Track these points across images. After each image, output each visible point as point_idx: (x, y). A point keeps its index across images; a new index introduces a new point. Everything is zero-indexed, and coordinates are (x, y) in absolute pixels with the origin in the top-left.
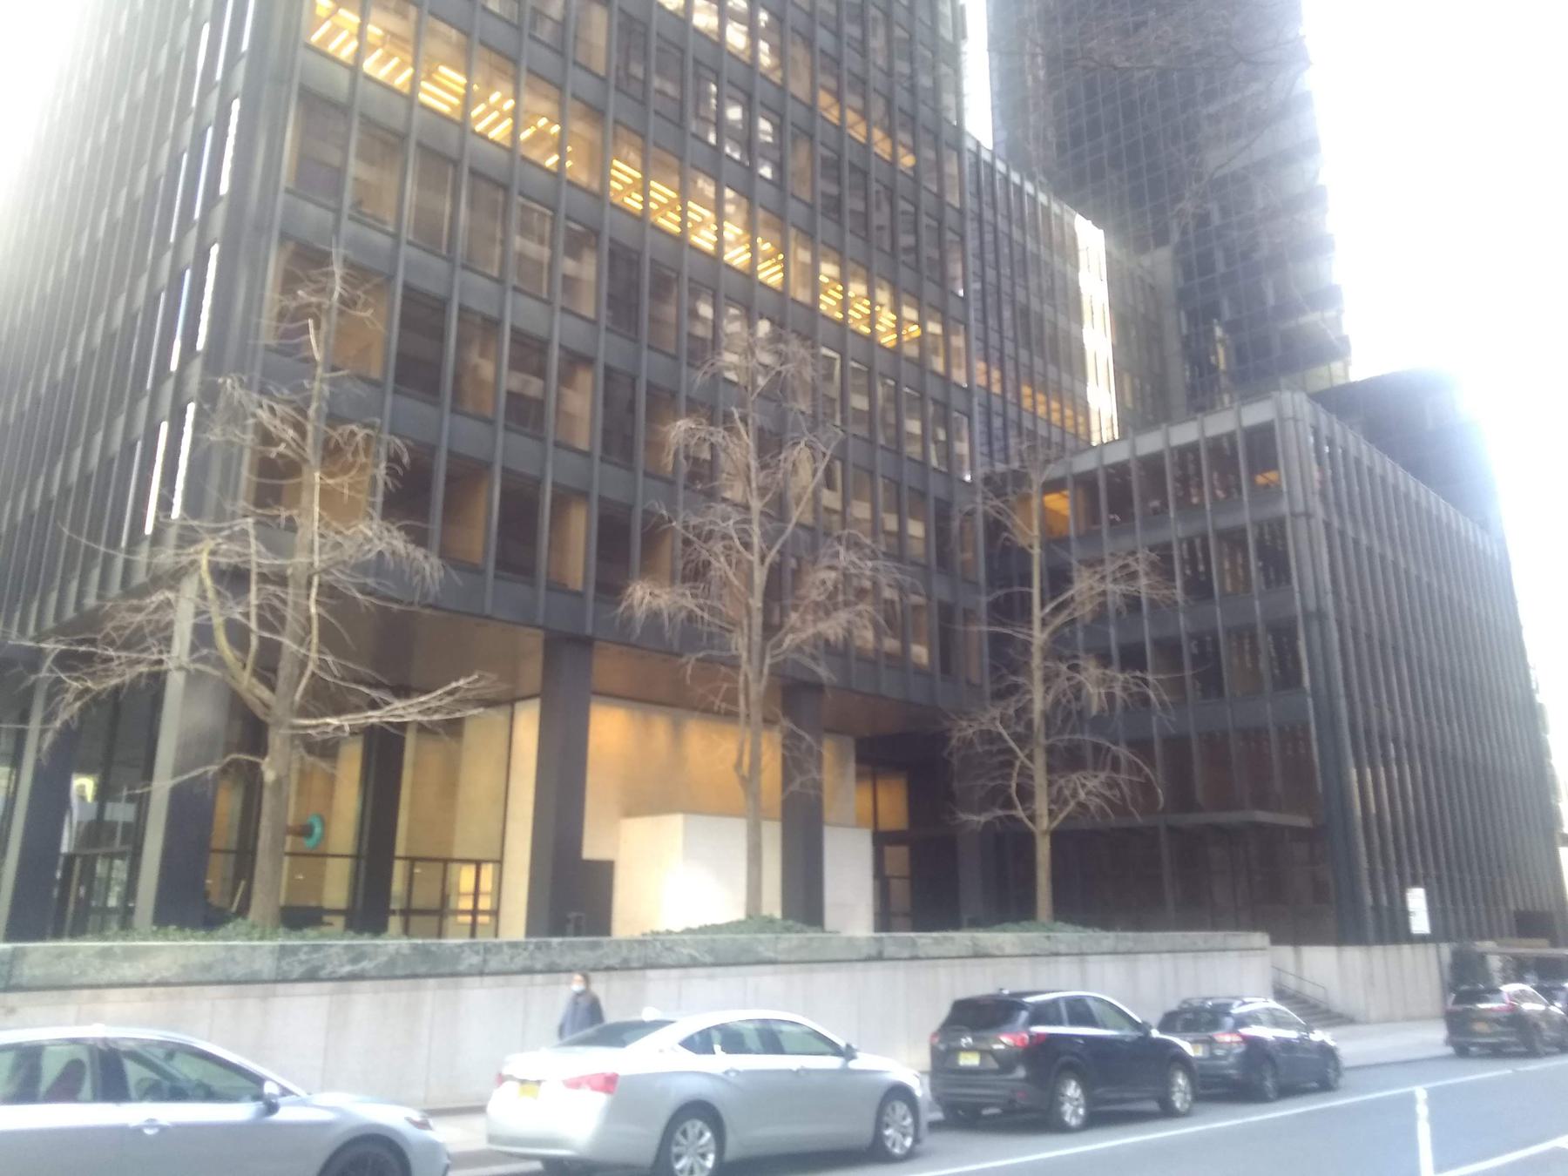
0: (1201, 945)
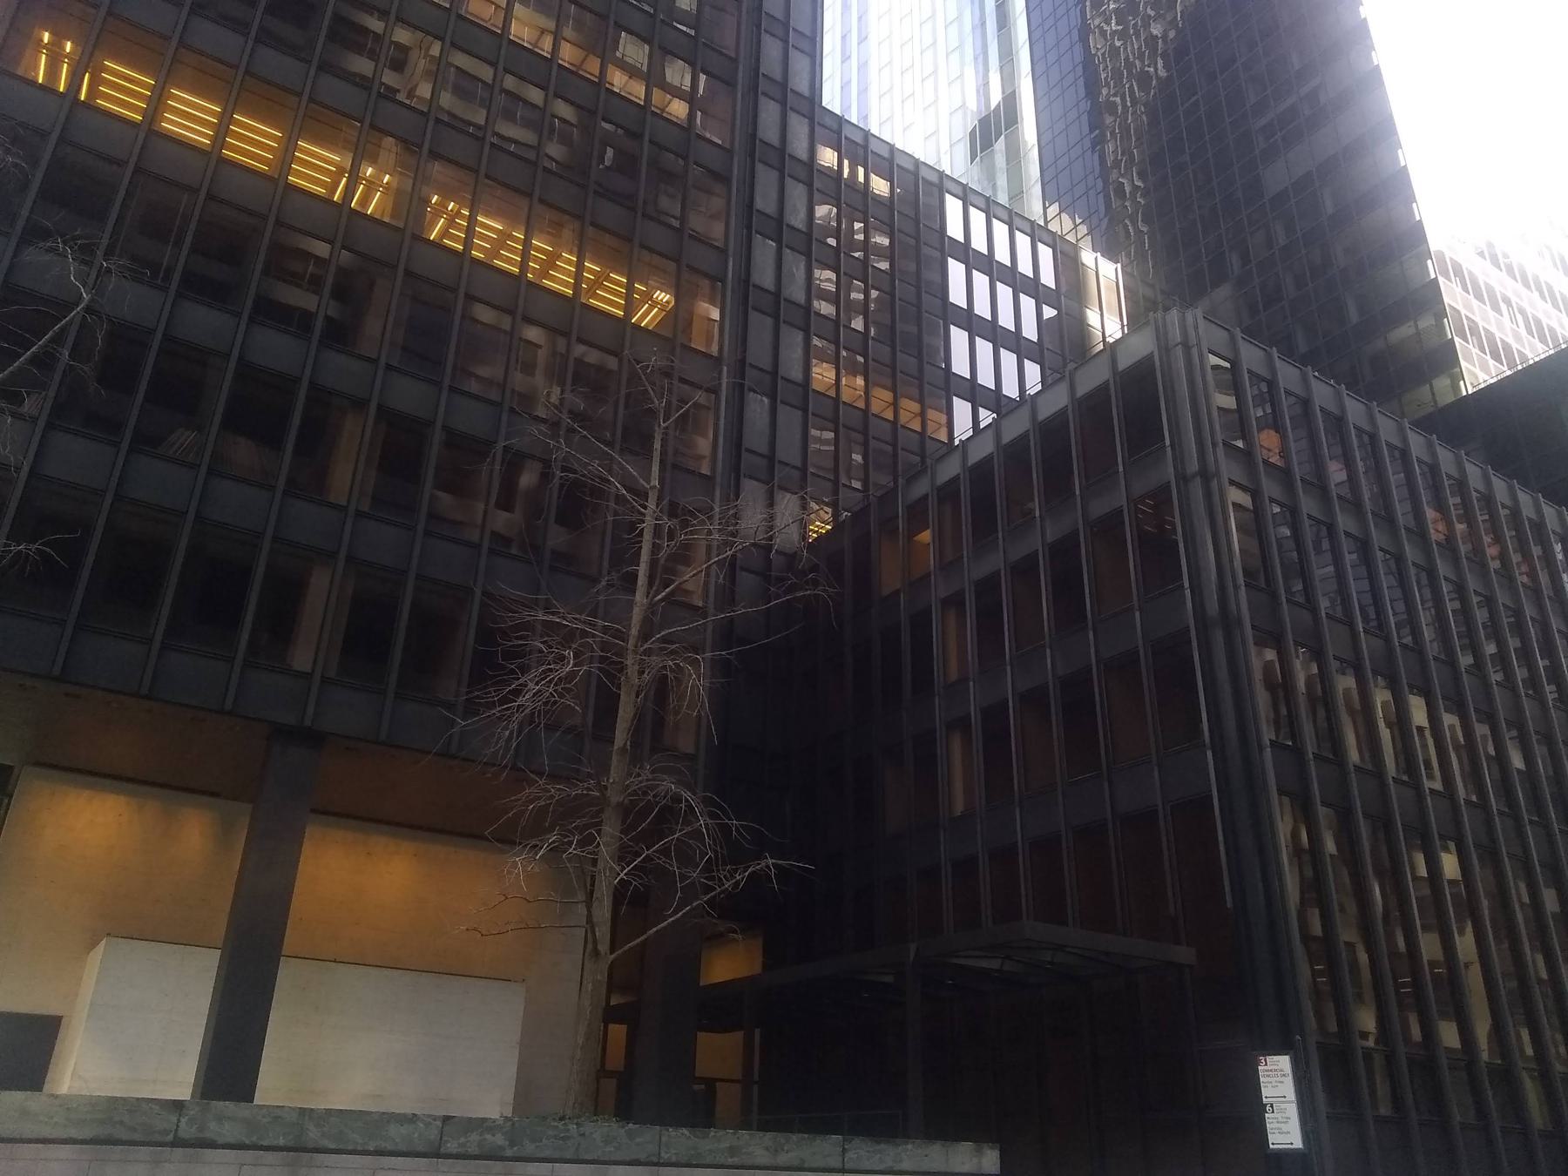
0: (761, 1156)
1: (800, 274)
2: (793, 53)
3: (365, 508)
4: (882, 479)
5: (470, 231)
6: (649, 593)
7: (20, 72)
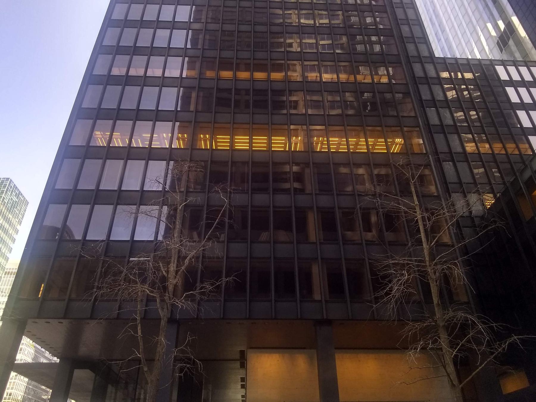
1: (448, 115)
2: (407, 10)
3: (322, 241)
4: (509, 179)
5: (328, 145)
6: (428, 243)
7: (198, 148)
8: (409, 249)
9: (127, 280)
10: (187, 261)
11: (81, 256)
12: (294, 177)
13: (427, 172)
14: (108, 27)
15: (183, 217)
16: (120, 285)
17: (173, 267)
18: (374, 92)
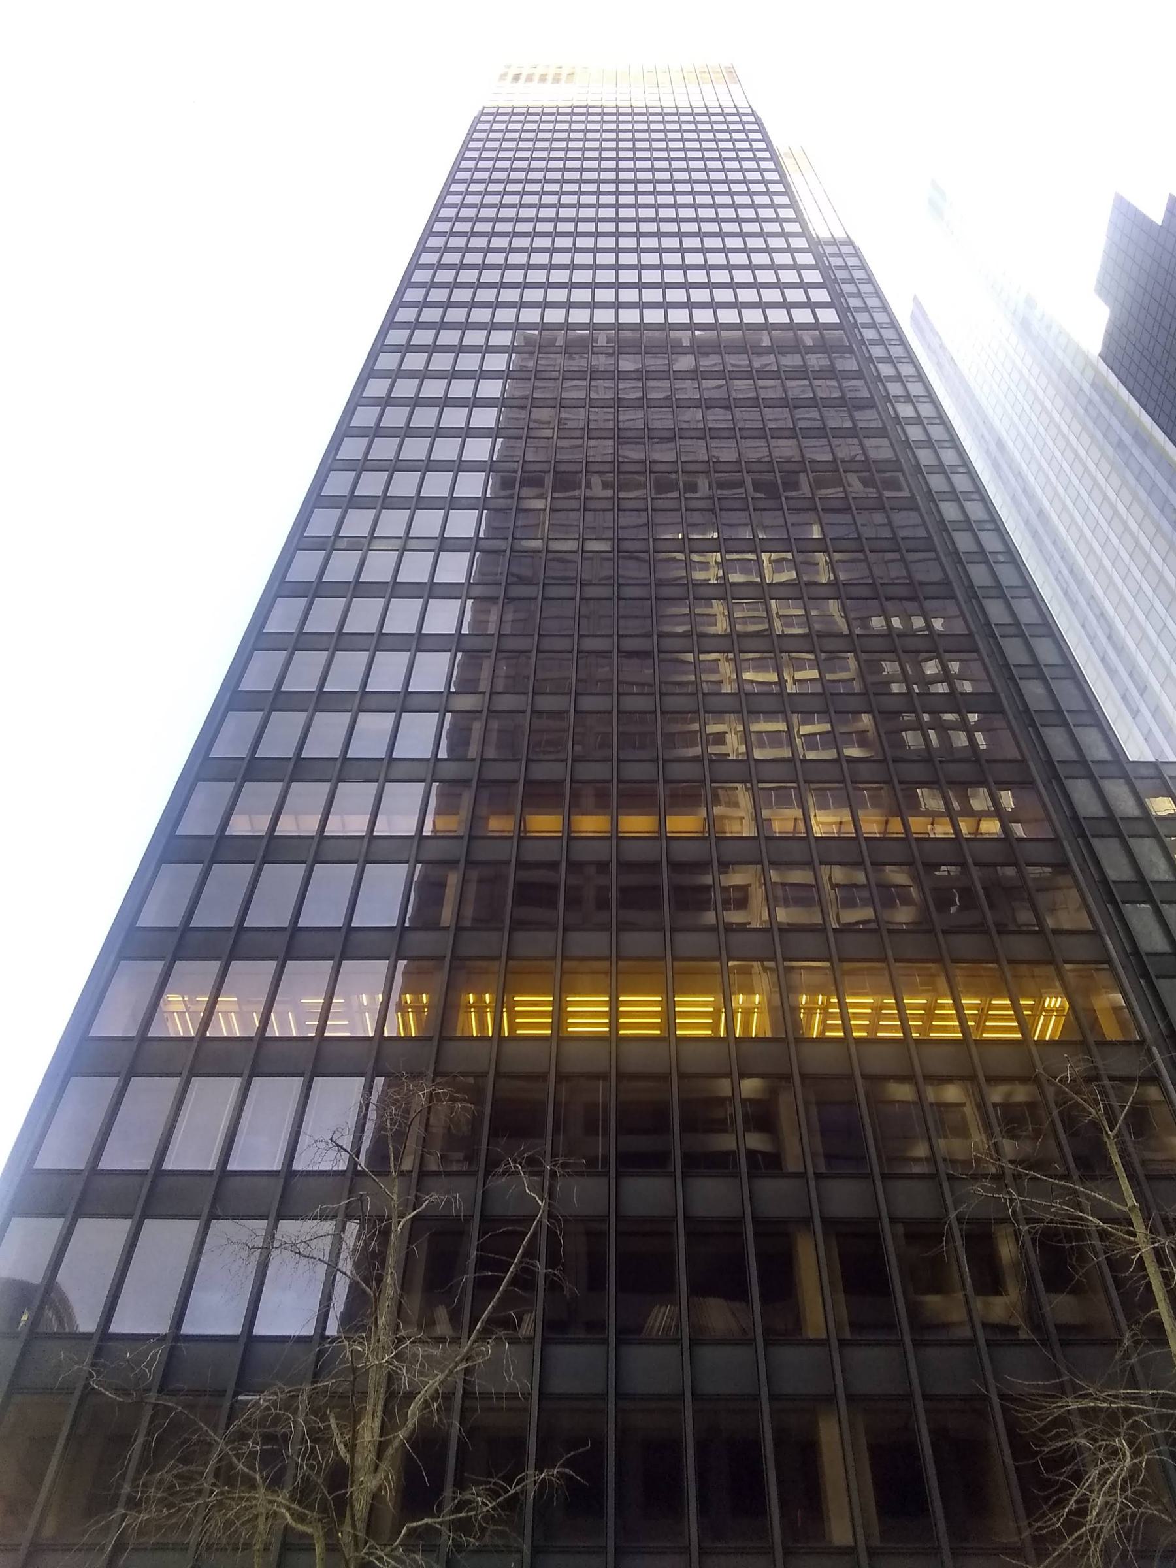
5: (844, 1016)
7: (459, 1034)
8: (1127, 1356)
9: (225, 1475)
10: (414, 1411)
11: (88, 1392)
12: (746, 1116)
13: (1153, 1093)
14: (231, 707)
15: (407, 1259)
16: (199, 1492)
17: (369, 1431)
18: (963, 865)
